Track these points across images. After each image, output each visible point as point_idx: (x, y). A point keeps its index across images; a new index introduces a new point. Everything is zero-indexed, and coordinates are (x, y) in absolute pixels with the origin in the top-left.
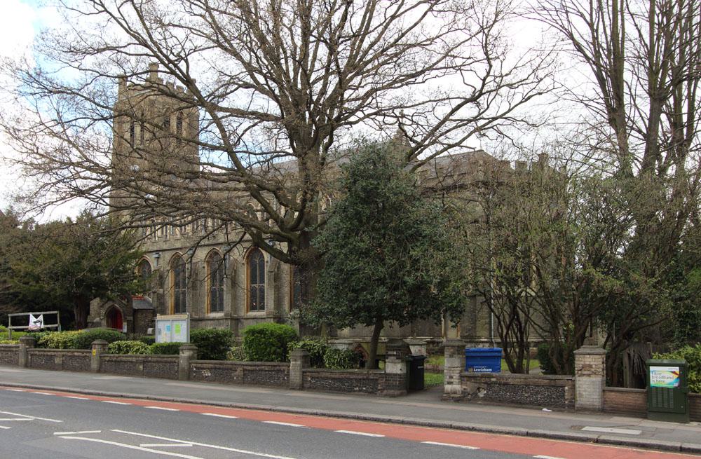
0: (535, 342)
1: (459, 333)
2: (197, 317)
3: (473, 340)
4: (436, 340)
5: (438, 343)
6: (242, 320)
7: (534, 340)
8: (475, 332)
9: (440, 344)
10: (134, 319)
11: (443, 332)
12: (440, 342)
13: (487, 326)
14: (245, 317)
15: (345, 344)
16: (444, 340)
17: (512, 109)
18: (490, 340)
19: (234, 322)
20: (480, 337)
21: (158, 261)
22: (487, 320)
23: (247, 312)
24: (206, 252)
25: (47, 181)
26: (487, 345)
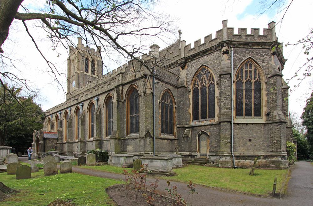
0: (264, 156)
1: (208, 150)
2: (72, 141)
3: (218, 154)
4: (193, 154)
5: (194, 156)
6: (87, 143)
7: (263, 154)
8: (220, 148)
9: (196, 156)
10: (44, 142)
11: (197, 148)
12: (195, 155)
13: (229, 144)
14: (88, 141)
15: (123, 157)
16: (198, 154)
17: (48, 63)
18: (230, 155)
19: (83, 143)
20: (223, 152)
21: (82, 107)
22: (229, 140)
23: (128, 134)
24: (105, 96)
25: (109, 31)
26: (229, 158)
